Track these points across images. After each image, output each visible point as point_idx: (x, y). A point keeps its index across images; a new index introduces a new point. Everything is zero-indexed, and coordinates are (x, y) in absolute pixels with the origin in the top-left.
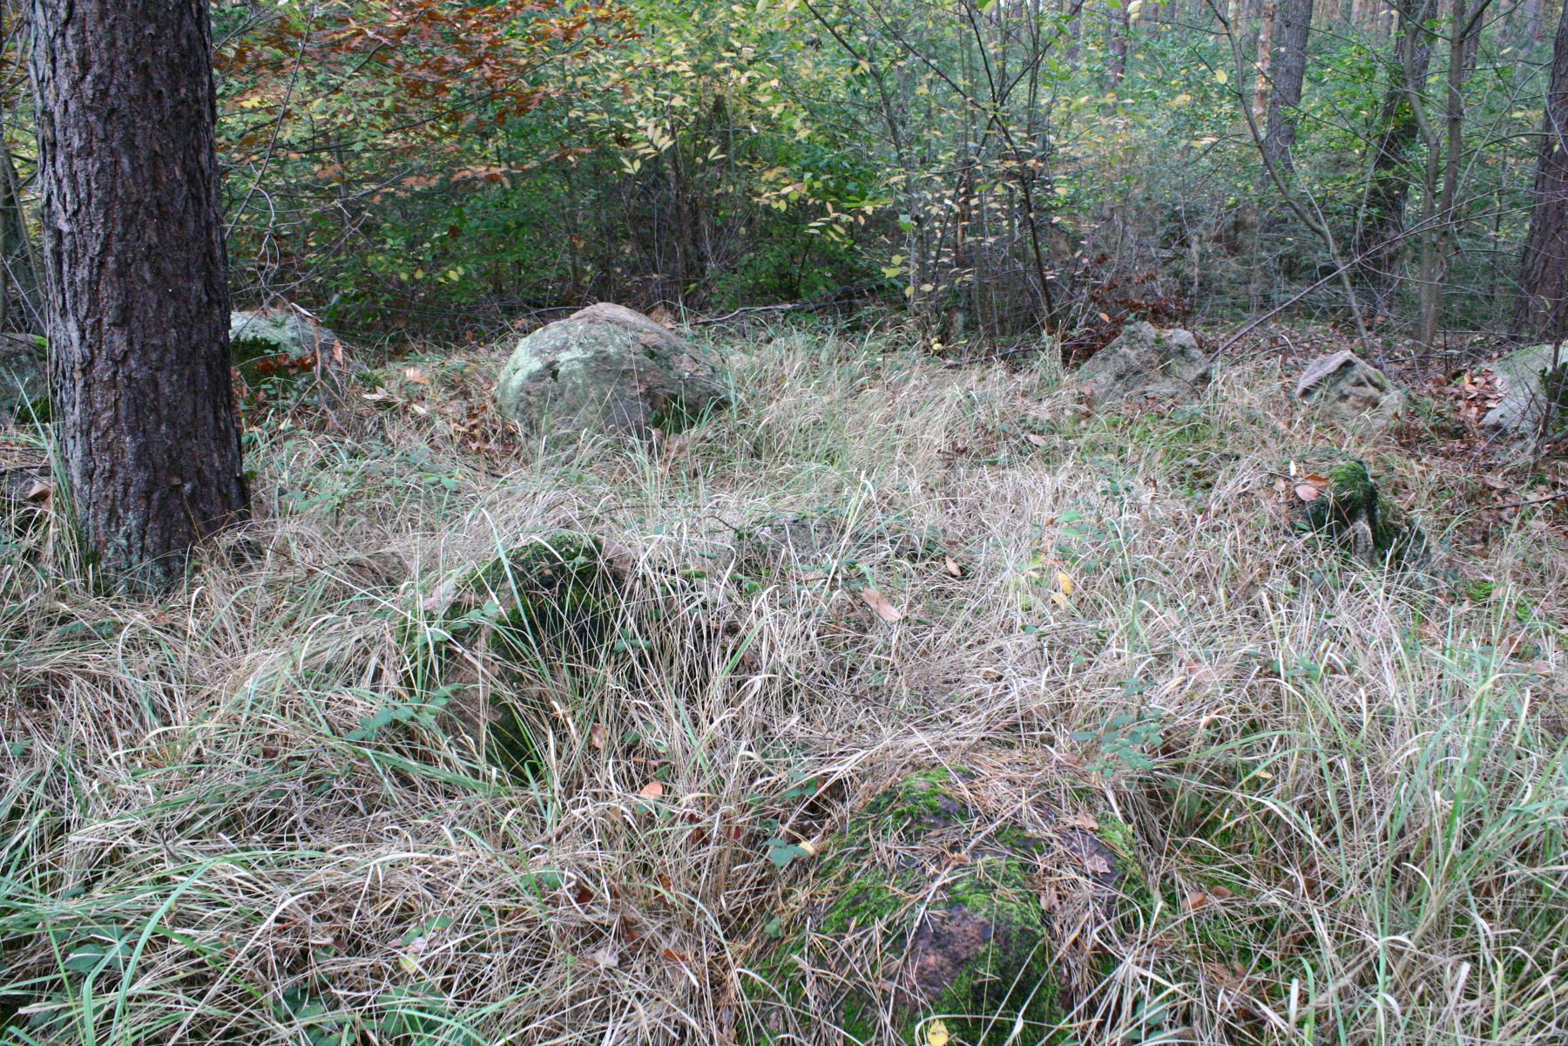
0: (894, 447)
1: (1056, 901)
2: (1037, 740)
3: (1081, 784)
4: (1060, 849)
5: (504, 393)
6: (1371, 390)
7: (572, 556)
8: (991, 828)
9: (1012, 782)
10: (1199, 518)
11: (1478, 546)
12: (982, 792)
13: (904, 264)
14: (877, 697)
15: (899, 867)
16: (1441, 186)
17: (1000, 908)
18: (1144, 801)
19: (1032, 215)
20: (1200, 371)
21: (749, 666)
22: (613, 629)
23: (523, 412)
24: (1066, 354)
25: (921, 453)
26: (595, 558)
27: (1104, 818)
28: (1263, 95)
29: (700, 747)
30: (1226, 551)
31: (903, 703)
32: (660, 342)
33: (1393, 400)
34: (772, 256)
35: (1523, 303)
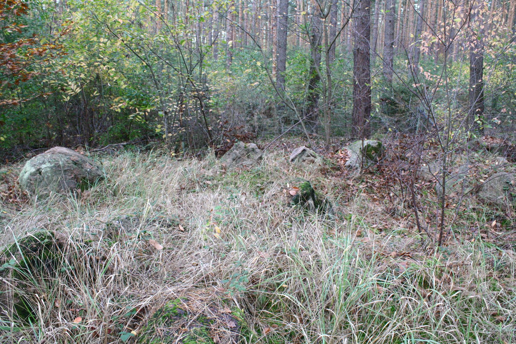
0: (161, 189)
1: (219, 339)
3: (225, 298)
4: (219, 321)
5: (21, 181)
6: (312, 158)
7: (43, 240)
8: (195, 317)
10: (260, 204)
11: (347, 203)
12: (191, 305)
13: (162, 127)
14: (156, 276)
15: (165, 335)
16: (327, 94)
18: (247, 300)
20: (259, 156)
21: (109, 271)
22: (60, 263)
23: (29, 187)
24: (216, 154)
26: (51, 239)
27: (233, 308)
28: (275, 68)
29: (94, 302)
30: (269, 214)
31: (165, 277)
32: (79, 159)
33: (319, 160)
34: (118, 127)
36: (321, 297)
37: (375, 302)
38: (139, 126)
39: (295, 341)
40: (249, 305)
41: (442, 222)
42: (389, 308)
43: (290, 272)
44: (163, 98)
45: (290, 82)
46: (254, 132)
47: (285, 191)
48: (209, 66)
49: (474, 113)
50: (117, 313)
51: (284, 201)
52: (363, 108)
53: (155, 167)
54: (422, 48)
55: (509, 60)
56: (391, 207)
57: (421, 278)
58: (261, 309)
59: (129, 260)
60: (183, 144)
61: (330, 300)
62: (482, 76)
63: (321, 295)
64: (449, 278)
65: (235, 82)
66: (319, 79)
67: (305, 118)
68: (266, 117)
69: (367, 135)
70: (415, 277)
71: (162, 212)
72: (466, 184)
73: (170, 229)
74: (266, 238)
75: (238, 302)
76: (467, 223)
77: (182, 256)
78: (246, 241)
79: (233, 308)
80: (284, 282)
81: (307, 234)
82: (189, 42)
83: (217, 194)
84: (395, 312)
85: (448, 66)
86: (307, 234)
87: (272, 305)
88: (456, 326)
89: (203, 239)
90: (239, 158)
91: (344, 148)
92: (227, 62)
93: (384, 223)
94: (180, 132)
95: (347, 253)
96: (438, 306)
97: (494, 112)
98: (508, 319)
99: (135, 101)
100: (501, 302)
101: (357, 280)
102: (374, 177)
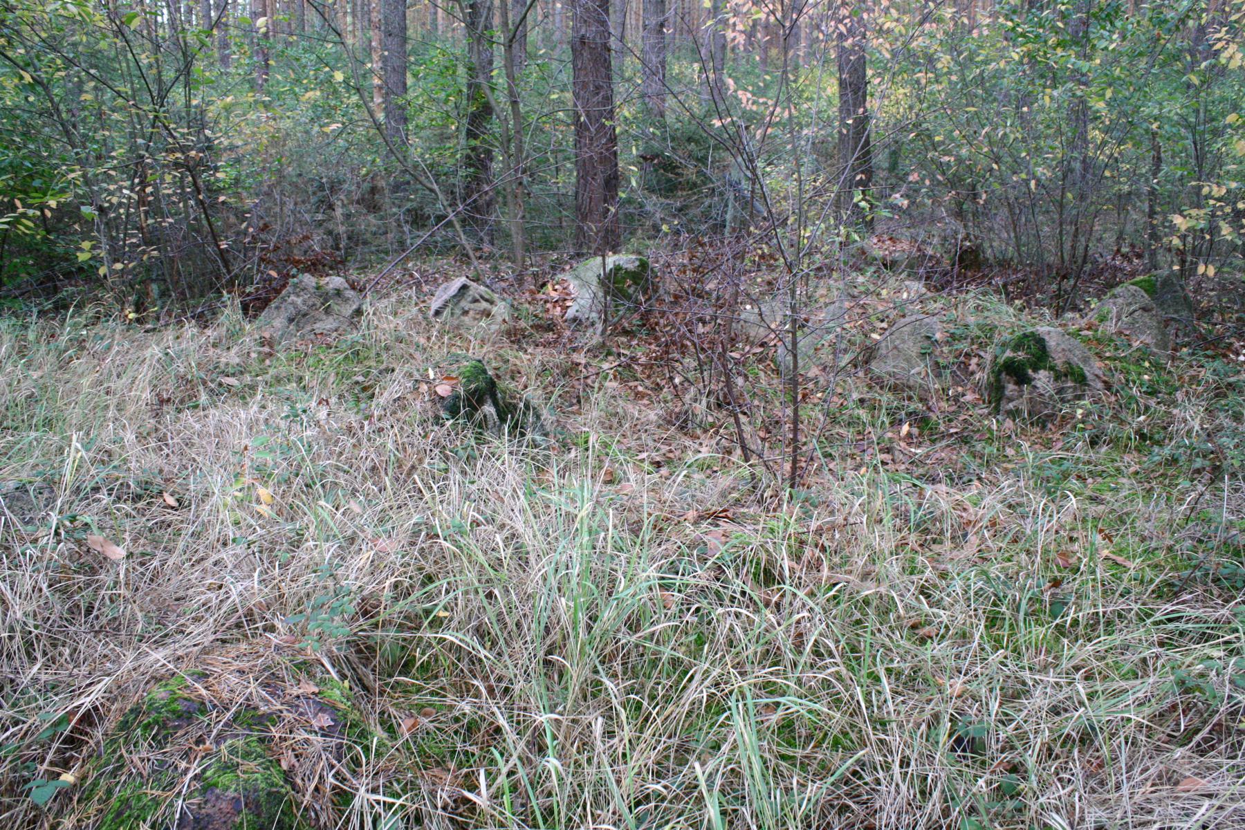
0: (107, 407)
1: (294, 760)
2: (261, 631)
3: (300, 658)
6: (484, 305)
8: (229, 715)
9: (241, 672)
10: (366, 423)
11: (575, 408)
12: (216, 687)
13: (94, 248)
14: (114, 627)
15: (154, 771)
16: (513, 149)
17: (246, 781)
18: (354, 658)
19: (201, 197)
20: (354, 307)
24: (245, 308)
25: (131, 409)
27: (323, 681)
28: (380, 88)
30: (390, 446)
31: (140, 626)
33: (501, 309)
35: (580, 228)
36: (533, 630)
37: (659, 627)
38: (28, 248)
39: (480, 740)
40: (362, 670)
41: (795, 435)
42: (691, 639)
43: (452, 579)
44: (91, 172)
45: (420, 122)
46: (338, 249)
47: (424, 387)
48: (209, 83)
49: (851, 184)
50: (14, 735)
51: (425, 411)
52: (600, 179)
53: (85, 352)
54: (730, 34)
55: (919, 64)
56: (677, 410)
57: (758, 564)
58: (390, 676)
59: (36, 594)
60: (154, 288)
61: (556, 636)
62: (865, 100)
63: (533, 626)
64: (819, 558)
65: (281, 125)
66: (491, 114)
67: (461, 207)
68: (365, 211)
69: (612, 243)
70: (744, 564)
71: (116, 463)
72: (843, 346)
73: (140, 505)
74: (387, 505)
75: (334, 666)
76: (849, 433)
77: (178, 569)
78: (339, 515)
79: (323, 681)
80: (440, 606)
81: (487, 486)
82: (151, 25)
83: (255, 408)
84: (706, 647)
85: (792, 78)
86: (487, 486)
87: (418, 664)
88: (838, 660)
89: (229, 522)
90: (305, 315)
91: (560, 276)
92: (255, 75)
93: (665, 448)
94: (145, 258)
95: (586, 521)
96: (798, 622)
97: (893, 181)
98: (942, 631)
99: (12, 179)
100: (928, 596)
101: (613, 581)
102: (634, 343)
